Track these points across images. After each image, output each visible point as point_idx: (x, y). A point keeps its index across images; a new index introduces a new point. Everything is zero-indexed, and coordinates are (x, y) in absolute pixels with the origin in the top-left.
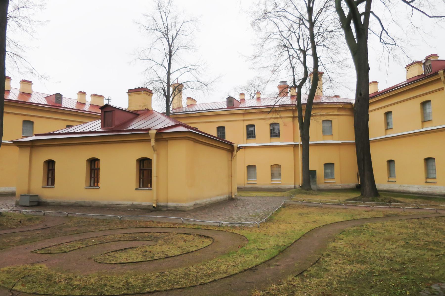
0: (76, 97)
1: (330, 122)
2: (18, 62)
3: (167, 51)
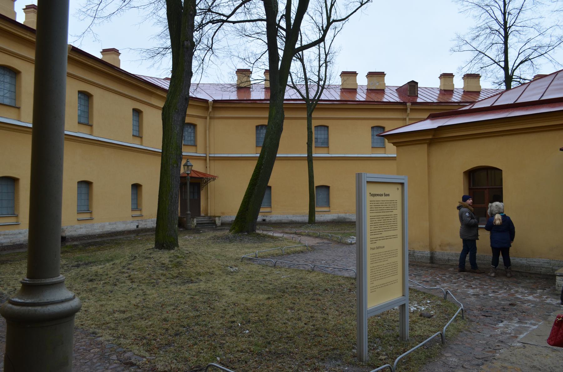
0: (436, 84)
1: (326, 128)
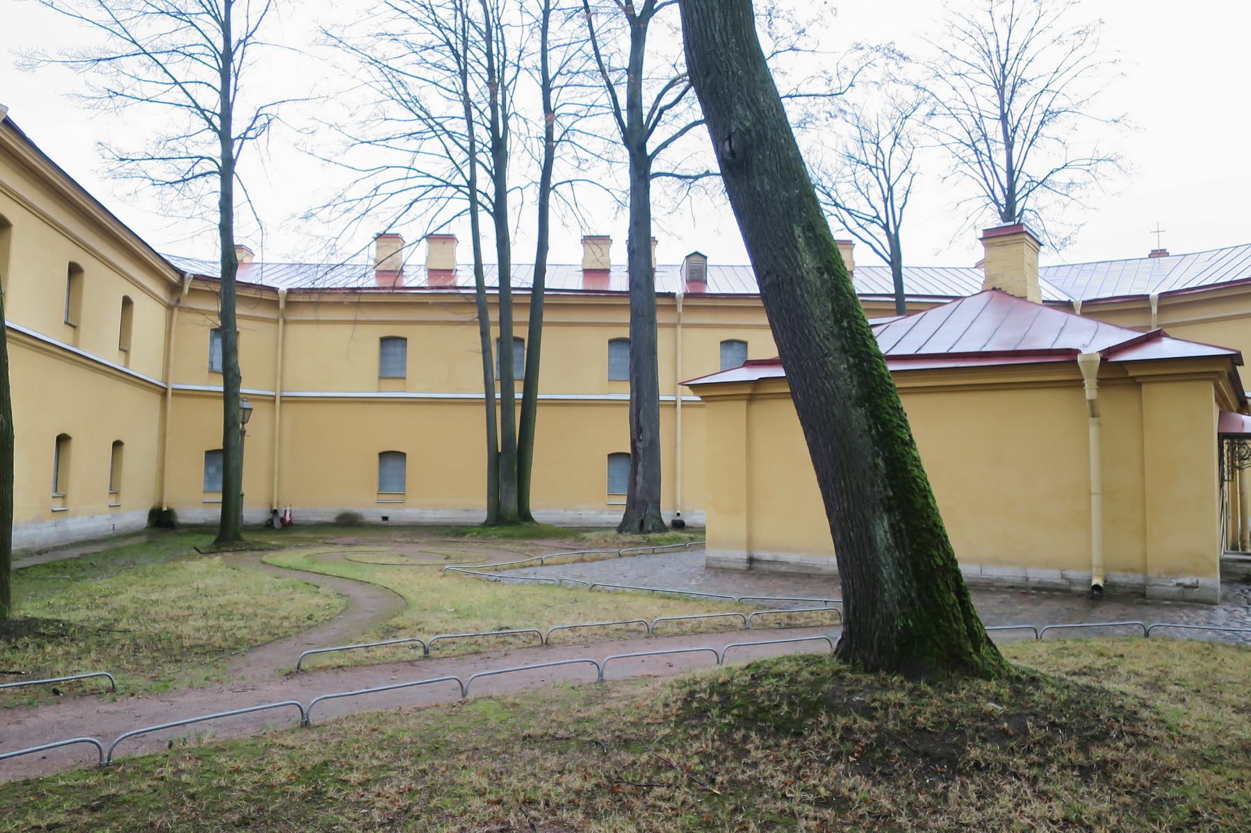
1: (743, 346)
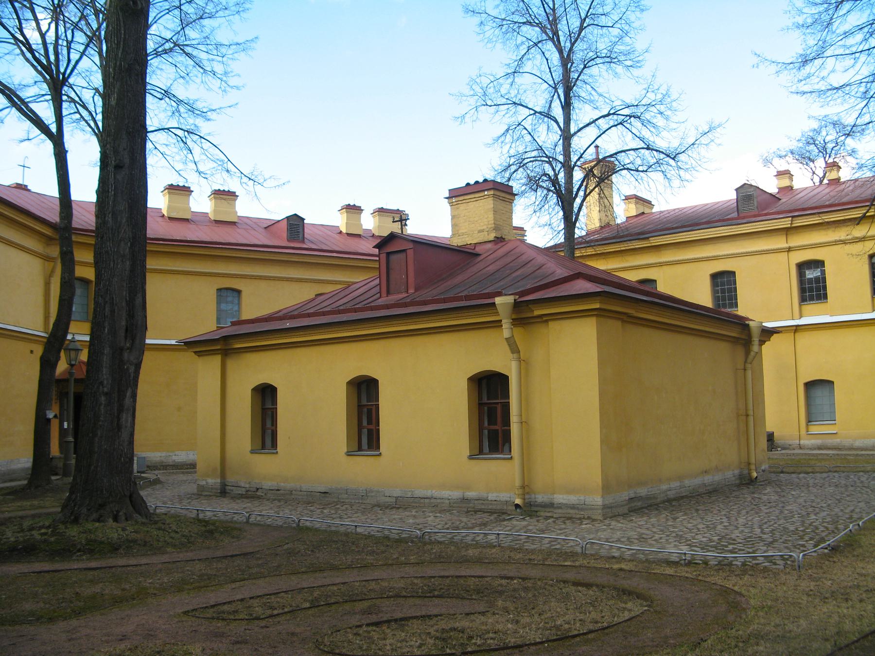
1: (235, 294)
2: (196, 150)
3: (558, 74)
